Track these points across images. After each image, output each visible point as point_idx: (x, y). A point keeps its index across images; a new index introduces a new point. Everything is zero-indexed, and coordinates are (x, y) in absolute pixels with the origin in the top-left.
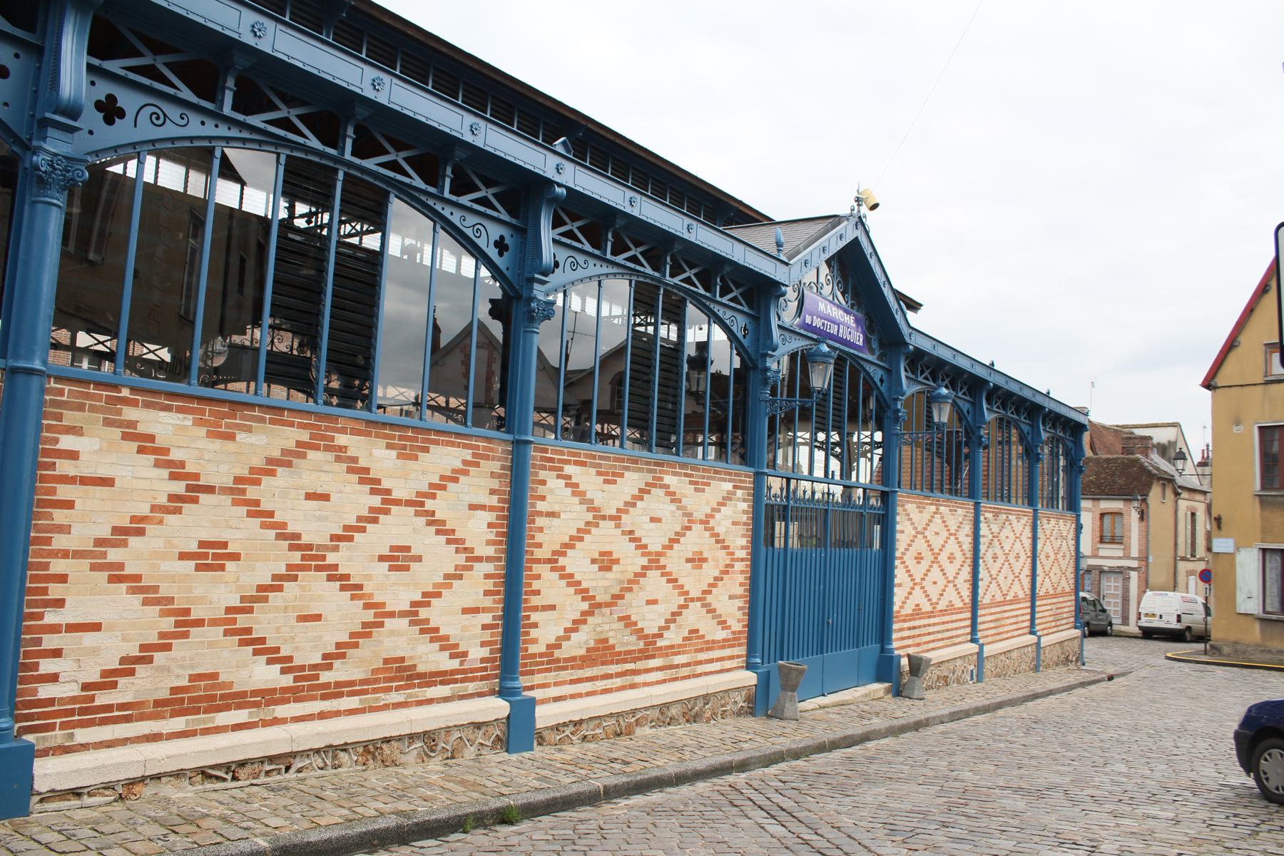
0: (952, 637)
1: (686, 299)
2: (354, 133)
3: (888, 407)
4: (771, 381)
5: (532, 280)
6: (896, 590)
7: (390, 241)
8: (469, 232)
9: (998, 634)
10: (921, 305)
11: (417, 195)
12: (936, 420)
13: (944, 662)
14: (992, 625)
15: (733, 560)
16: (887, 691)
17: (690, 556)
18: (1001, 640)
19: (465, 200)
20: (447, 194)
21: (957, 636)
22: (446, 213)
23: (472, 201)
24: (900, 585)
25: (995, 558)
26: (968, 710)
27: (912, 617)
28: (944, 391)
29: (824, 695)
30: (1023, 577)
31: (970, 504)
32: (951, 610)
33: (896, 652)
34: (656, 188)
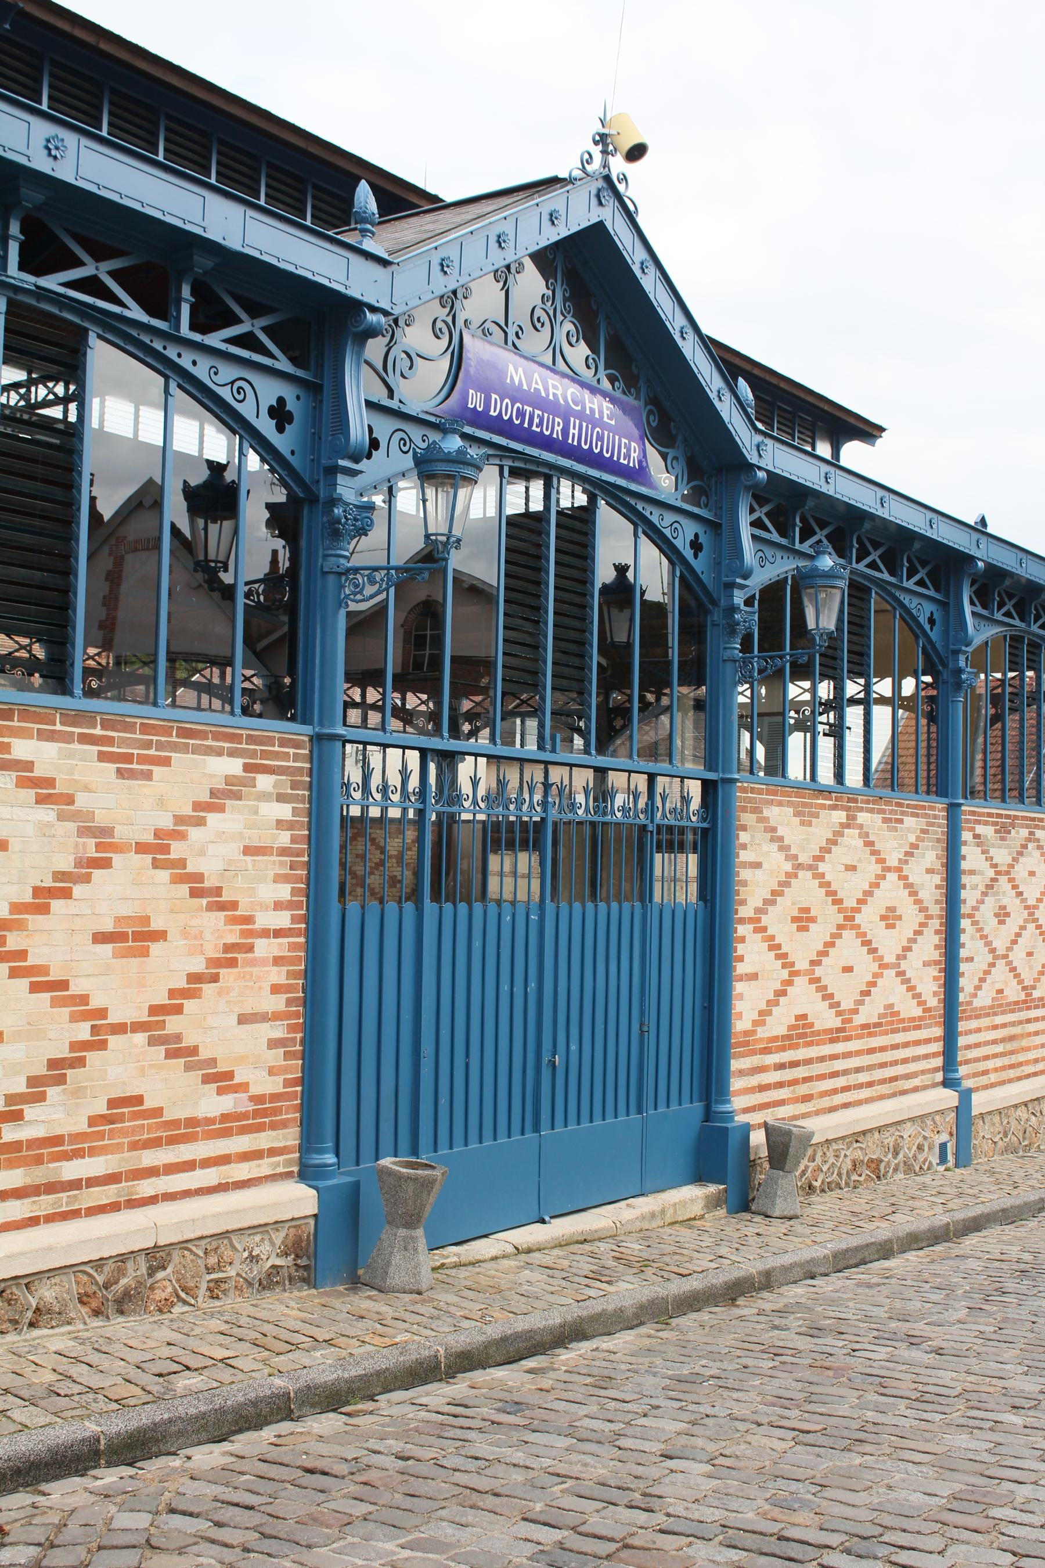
0: (894, 1079)
1: (87, 330)
2: (192, 295)
3: (714, 602)
4: (741, 629)
5: (333, 471)
6: (739, 987)
7: (175, 436)
8: (225, 393)
9: (1012, 1066)
10: (882, 429)
11: (134, 333)
12: (811, 624)
13: (870, 1131)
14: (999, 1048)
15: (251, 934)
16: (714, 1203)
17: (108, 926)
18: (1019, 1079)
19: (214, 340)
20: (185, 331)
21: (907, 1077)
22: (185, 362)
23: (226, 341)
24: (970, 959)
25: (1002, 915)
26: (890, 1241)
27: (992, 1011)
28: (827, 562)
29: (543, 1221)
30: (983, 958)
31: (938, 808)
32: (892, 1023)
33: (741, 1119)
34: (275, 184)
